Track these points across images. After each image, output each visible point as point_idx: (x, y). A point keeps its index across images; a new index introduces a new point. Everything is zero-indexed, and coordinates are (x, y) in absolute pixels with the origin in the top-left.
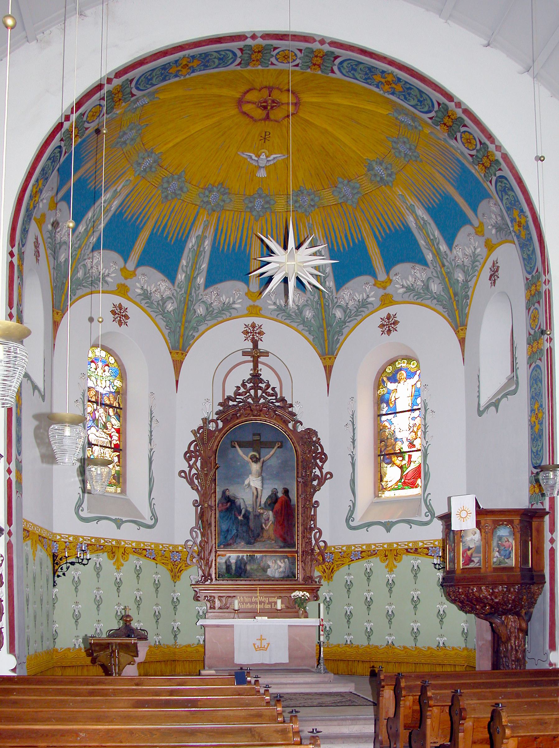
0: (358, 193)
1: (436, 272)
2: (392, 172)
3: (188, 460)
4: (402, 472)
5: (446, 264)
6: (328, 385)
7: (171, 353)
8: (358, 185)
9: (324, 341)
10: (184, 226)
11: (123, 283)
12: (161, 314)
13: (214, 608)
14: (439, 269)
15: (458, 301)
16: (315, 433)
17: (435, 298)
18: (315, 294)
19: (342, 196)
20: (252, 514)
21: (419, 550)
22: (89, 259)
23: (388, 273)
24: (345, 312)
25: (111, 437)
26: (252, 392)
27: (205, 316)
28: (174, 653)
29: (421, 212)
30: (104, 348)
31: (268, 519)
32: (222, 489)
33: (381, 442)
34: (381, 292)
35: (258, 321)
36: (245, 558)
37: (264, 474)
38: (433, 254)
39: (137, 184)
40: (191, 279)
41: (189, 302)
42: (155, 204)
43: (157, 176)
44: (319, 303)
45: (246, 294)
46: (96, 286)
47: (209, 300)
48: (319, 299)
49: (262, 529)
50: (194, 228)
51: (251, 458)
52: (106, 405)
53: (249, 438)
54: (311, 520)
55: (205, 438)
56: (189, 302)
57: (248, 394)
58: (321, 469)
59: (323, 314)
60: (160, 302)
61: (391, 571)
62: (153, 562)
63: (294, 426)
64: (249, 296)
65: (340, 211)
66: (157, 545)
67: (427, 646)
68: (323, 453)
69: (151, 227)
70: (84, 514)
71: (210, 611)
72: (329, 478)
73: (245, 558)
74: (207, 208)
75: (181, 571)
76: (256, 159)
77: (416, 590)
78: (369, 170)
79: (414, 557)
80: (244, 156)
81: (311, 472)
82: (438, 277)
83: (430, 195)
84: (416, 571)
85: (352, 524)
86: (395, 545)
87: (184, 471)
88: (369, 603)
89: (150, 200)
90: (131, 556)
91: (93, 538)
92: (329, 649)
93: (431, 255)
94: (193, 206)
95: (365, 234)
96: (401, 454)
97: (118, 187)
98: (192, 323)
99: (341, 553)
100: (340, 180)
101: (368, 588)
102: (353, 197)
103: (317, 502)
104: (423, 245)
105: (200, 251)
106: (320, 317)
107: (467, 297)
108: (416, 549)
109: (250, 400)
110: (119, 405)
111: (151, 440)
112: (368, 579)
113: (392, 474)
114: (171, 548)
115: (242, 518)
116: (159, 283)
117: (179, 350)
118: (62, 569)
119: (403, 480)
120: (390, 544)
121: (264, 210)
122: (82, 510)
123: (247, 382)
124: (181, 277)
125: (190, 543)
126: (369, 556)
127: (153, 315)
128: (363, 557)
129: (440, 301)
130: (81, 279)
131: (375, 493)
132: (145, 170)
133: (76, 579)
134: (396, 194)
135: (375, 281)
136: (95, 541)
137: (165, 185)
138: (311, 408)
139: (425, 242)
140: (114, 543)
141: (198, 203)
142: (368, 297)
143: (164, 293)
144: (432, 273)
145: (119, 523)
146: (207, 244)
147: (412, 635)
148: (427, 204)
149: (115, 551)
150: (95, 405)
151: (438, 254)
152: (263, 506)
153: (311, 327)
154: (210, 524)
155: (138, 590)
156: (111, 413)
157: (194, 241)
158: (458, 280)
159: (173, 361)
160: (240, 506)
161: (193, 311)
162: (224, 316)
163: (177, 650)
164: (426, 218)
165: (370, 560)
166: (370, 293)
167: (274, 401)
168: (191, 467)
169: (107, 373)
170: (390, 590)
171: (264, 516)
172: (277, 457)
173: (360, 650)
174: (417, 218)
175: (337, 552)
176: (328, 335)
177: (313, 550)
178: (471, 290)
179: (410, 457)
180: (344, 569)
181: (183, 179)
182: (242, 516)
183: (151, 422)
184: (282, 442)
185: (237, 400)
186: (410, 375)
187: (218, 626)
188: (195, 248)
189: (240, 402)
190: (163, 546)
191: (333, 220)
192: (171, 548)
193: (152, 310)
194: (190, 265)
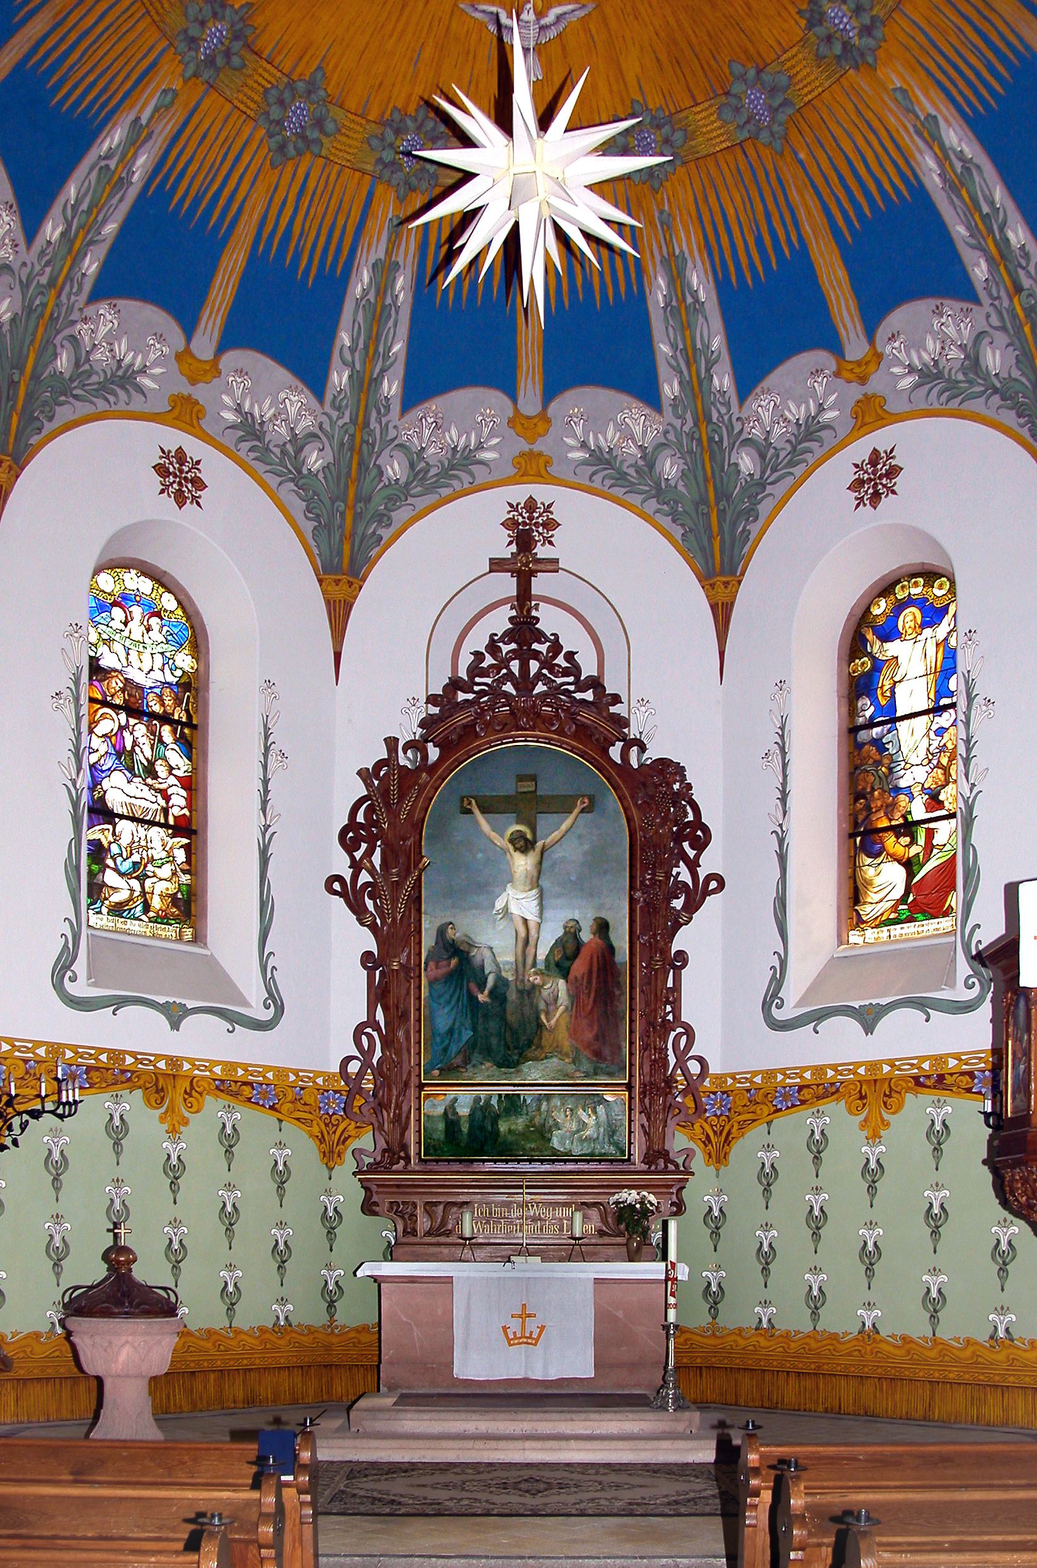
0: (786, 103)
1: (1000, 313)
2: (872, 18)
3: (349, 847)
4: (910, 875)
6: (722, 655)
7: (320, 581)
8: (783, 80)
9: (711, 537)
10: (337, 234)
12: (292, 480)
13: (414, 1233)
14: (1006, 303)
16: (680, 770)
17: (996, 391)
18: (685, 412)
19: (744, 119)
20: (512, 987)
21: (949, 1080)
22: (85, 320)
23: (870, 334)
24: (762, 456)
25: (167, 798)
26: (515, 666)
27: (407, 484)
28: (328, 1348)
29: (955, 136)
30: (147, 571)
31: (556, 999)
32: (438, 923)
33: (856, 800)
34: (855, 392)
35: (542, 493)
36: (494, 1102)
37: (545, 883)
38: (990, 260)
39: (198, 105)
40: (365, 384)
41: (365, 447)
42: (253, 168)
43: (250, 82)
44: (696, 436)
45: (511, 422)
46: (112, 399)
47: (415, 440)
48: (696, 424)
49: (540, 1025)
50: (365, 241)
51: (511, 841)
52: (153, 715)
53: (507, 787)
54: (668, 1002)
55: (394, 788)
56: (365, 447)
57: (504, 671)
58: (693, 866)
59: (708, 465)
60: (289, 446)
61: (874, 1137)
62: (271, 1119)
63: (625, 754)
64: (519, 427)
65: (742, 167)
66: (281, 1072)
67: (963, 1336)
68: (699, 824)
69: (250, 238)
70: (80, 989)
71: (405, 1240)
72: (714, 891)
73: (494, 1102)
74: (394, 183)
75: (346, 1139)
77: (938, 1187)
78: (811, 25)
79: (935, 1098)
80: (478, 15)
81: (668, 875)
82: (1003, 328)
83: (978, 74)
84: (938, 1137)
85: (778, 1015)
86: (886, 1068)
87: (339, 878)
88: (816, 1222)
89: (238, 159)
90: (209, 1099)
91: (102, 1051)
92: (717, 1342)
93: (983, 264)
94: (358, 174)
96: (908, 828)
97: (141, 111)
98: (373, 504)
99: (748, 1091)
100: (738, 69)
101: (815, 1182)
102: (773, 119)
103: (681, 954)
104: (963, 238)
105: (384, 307)
106: (700, 473)
108: (941, 1077)
109: (508, 688)
110: (189, 717)
111: (264, 803)
112: (817, 1159)
113: (887, 879)
114: (320, 1081)
115: (487, 1000)
116: (282, 395)
117: (342, 573)
118: (10, 1128)
119: (911, 898)
120: (874, 1066)
122: (73, 979)
123: (502, 640)
124: (339, 378)
125: (354, 1067)
126: (819, 1098)
127: (273, 481)
128: (803, 1102)
129: (1011, 398)
130: (67, 376)
131: (839, 936)
132: (210, 61)
133: (56, 1155)
134: (886, 89)
135: (838, 364)
136: (109, 1058)
137: (276, 113)
138: (675, 709)
139: (968, 228)
140: (162, 1065)
141: (369, 167)
142: (821, 408)
143: (297, 422)
144: (988, 316)
145: (175, 1015)
147: (925, 1307)
148: (969, 104)
149: (166, 1086)
150: (123, 717)
151: (1002, 256)
152: (541, 966)
153: (676, 502)
154: (404, 1016)
155: (229, 1186)
156: (168, 737)
159: (328, 603)
160: (482, 967)
161: (374, 472)
162: (455, 483)
163: (335, 1340)
164: (968, 153)
165: (821, 1108)
167: (572, 688)
168: (357, 867)
169: (156, 635)
170: (872, 1189)
171: (545, 993)
172: (580, 837)
173: (793, 1345)
174: (944, 156)
175: (739, 1089)
176: (722, 513)
177: (670, 1081)
179: (930, 834)
180: (756, 1134)
181: (322, 93)
182: (486, 992)
183: (265, 755)
184: (592, 799)
185: (476, 688)
186: (933, 615)
187: (412, 1280)
188: (371, 297)
189: (482, 693)
190: (297, 1076)
191: (724, 194)
192: (320, 1081)
193: (269, 468)
194: (361, 346)
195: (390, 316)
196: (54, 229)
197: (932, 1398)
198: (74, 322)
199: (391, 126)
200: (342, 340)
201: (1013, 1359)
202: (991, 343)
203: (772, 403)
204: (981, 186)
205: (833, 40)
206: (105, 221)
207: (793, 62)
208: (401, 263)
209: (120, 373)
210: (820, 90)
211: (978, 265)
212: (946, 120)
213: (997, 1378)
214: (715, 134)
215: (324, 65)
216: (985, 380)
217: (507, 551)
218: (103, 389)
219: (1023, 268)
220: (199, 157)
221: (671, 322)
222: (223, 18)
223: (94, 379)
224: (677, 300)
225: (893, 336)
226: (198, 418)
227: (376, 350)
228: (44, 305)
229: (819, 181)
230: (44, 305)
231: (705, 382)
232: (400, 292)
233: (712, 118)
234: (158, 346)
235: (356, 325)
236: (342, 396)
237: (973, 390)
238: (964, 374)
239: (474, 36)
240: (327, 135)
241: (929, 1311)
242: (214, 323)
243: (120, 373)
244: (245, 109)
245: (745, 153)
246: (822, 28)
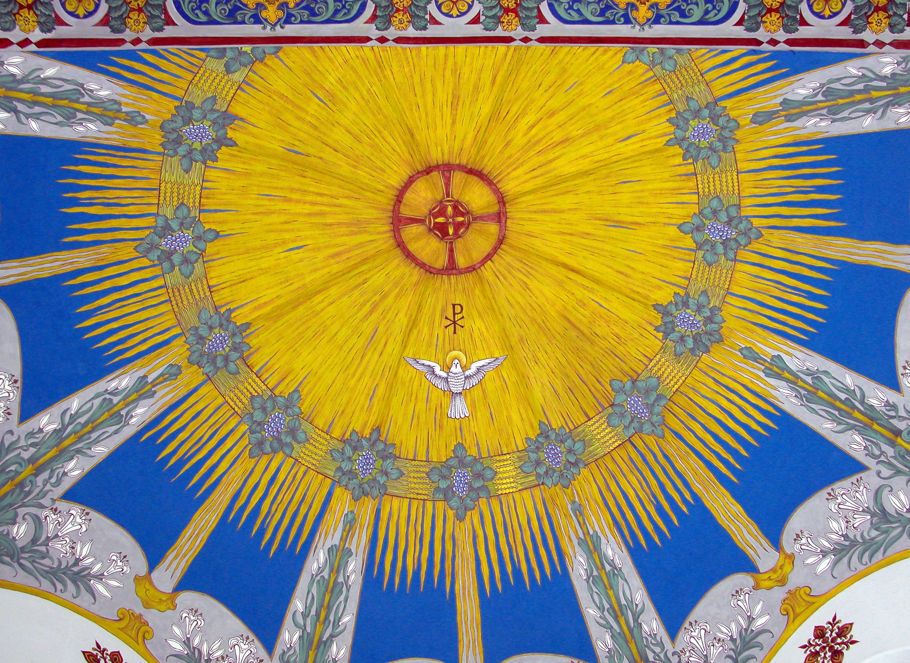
0: (660, 397)
11: (137, 612)
14: (890, 451)
19: (628, 421)
23: (776, 543)
34: (779, 594)
39: (195, 390)
46: (59, 586)
74: (350, 487)
76: (444, 375)
78: (666, 335)
82: (898, 472)
94: (320, 477)
95: (698, 488)
105: (336, 583)
116: (234, 642)
121: (474, 495)
137: (258, 416)
141: (331, 473)
144: (878, 473)
146: (354, 569)
151: (872, 419)
157: (322, 559)
166: (751, 609)
174: (793, 380)
181: (297, 410)
188: (326, 574)
194: (313, 612)
195: (341, 592)
196: (49, 424)
198: (42, 507)
199: (350, 445)
200: (296, 606)
202: (891, 490)
203: (703, 632)
204: (832, 384)
205: (686, 338)
206: (97, 441)
207: (659, 366)
208: (353, 551)
209: (76, 569)
210: (683, 378)
212: (788, 353)
214: (607, 438)
215: (300, 389)
217: (499, 186)
218: (56, 574)
220: (191, 427)
221: (595, 589)
222: (227, 330)
223: (47, 561)
224: (597, 569)
225: (798, 535)
226: (144, 637)
227: (327, 617)
228: (18, 473)
229: (698, 446)
230: (18, 473)
231: (636, 631)
232: (351, 574)
233: (603, 427)
234: (120, 564)
235: (310, 595)
236: (292, 652)
237: (891, 536)
238: (876, 529)
239: (416, 383)
240: (299, 443)
242: (179, 564)
243: (76, 569)
244: (234, 406)
245: (634, 445)
246: (676, 334)
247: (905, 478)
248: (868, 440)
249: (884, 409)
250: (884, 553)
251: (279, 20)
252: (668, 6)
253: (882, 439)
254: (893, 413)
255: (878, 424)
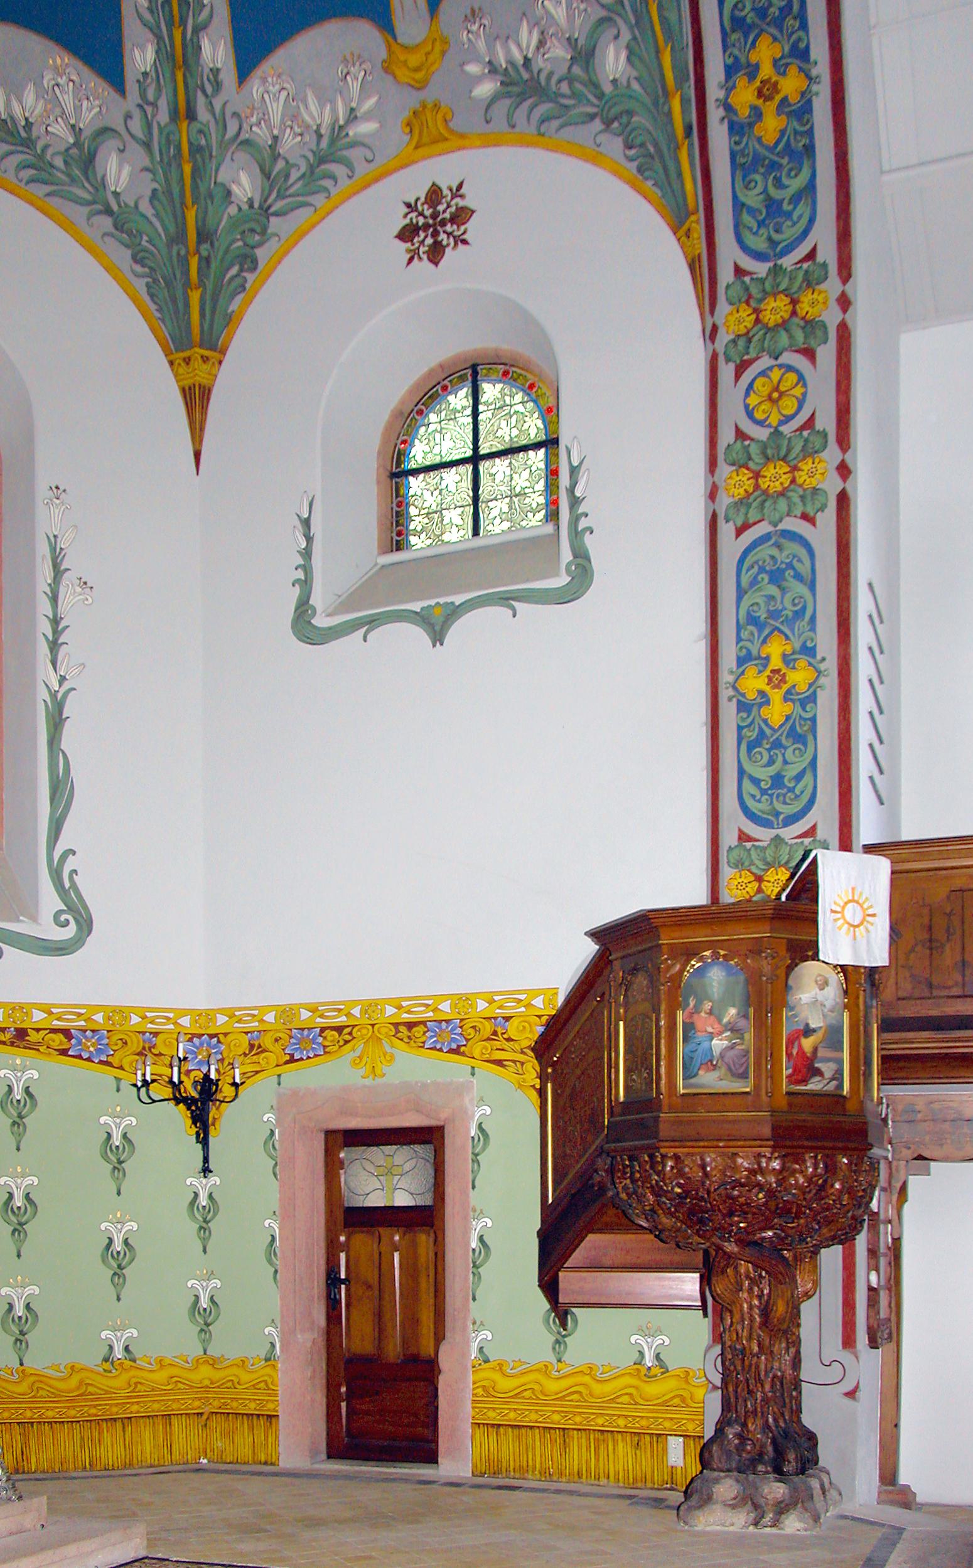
5: (203, 115)
14: (163, 117)
15: (208, 260)
17: (108, 211)
21: (33, 1037)
40: (180, 59)
82: (147, 145)
93: (150, 54)
107: (248, 262)
144: (128, 116)
158: (229, 193)
178: (273, 245)
197: (25, 1443)
201: (136, 1383)
202: (122, 151)
211: (143, 50)
213: (115, 1409)
216: (97, 189)
219: (206, 96)
238: (66, 163)
241: (11, 1334)
247: (147, 163)
248: (157, 71)
249: (206, 71)
250: (48, 195)
251: (743, 695)
252: (765, 721)
253: (171, 92)
254: (209, 89)
255: (184, 76)
